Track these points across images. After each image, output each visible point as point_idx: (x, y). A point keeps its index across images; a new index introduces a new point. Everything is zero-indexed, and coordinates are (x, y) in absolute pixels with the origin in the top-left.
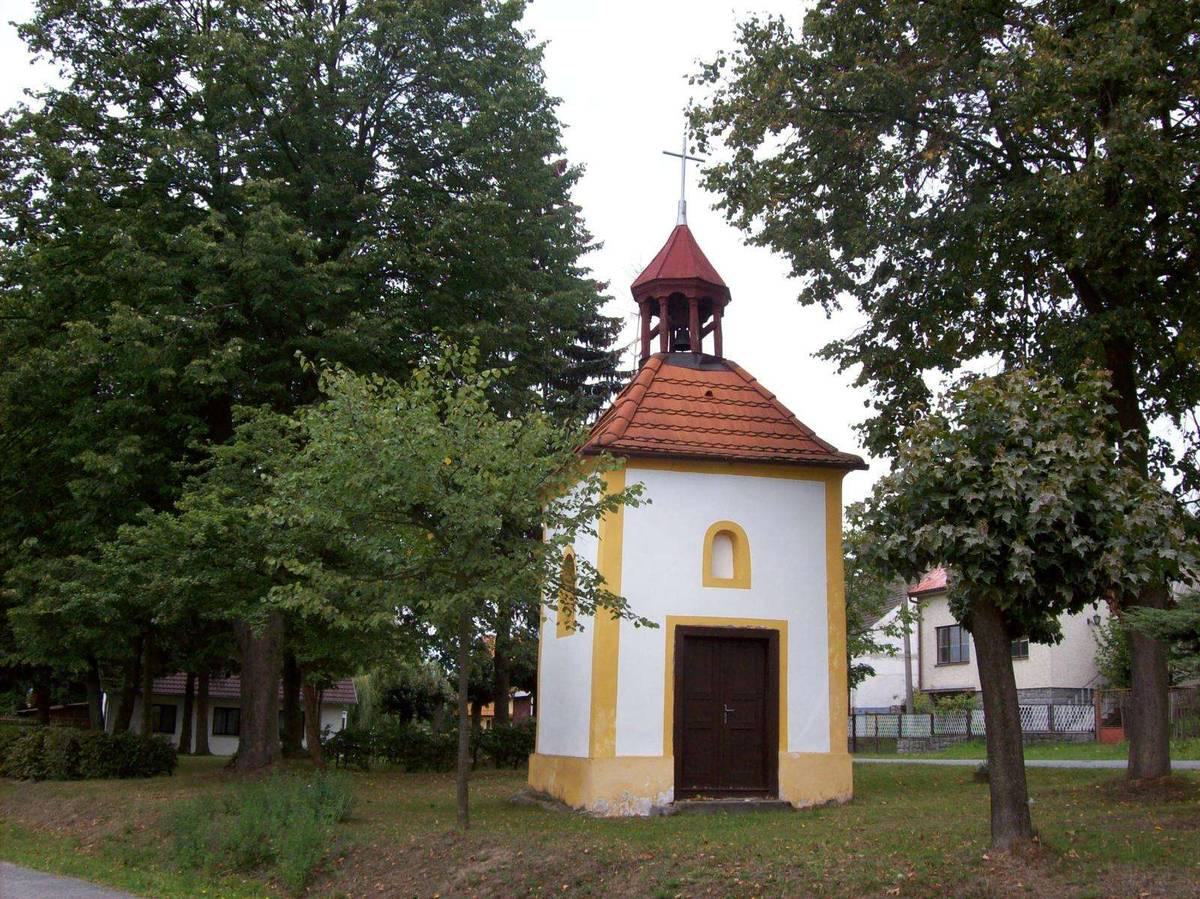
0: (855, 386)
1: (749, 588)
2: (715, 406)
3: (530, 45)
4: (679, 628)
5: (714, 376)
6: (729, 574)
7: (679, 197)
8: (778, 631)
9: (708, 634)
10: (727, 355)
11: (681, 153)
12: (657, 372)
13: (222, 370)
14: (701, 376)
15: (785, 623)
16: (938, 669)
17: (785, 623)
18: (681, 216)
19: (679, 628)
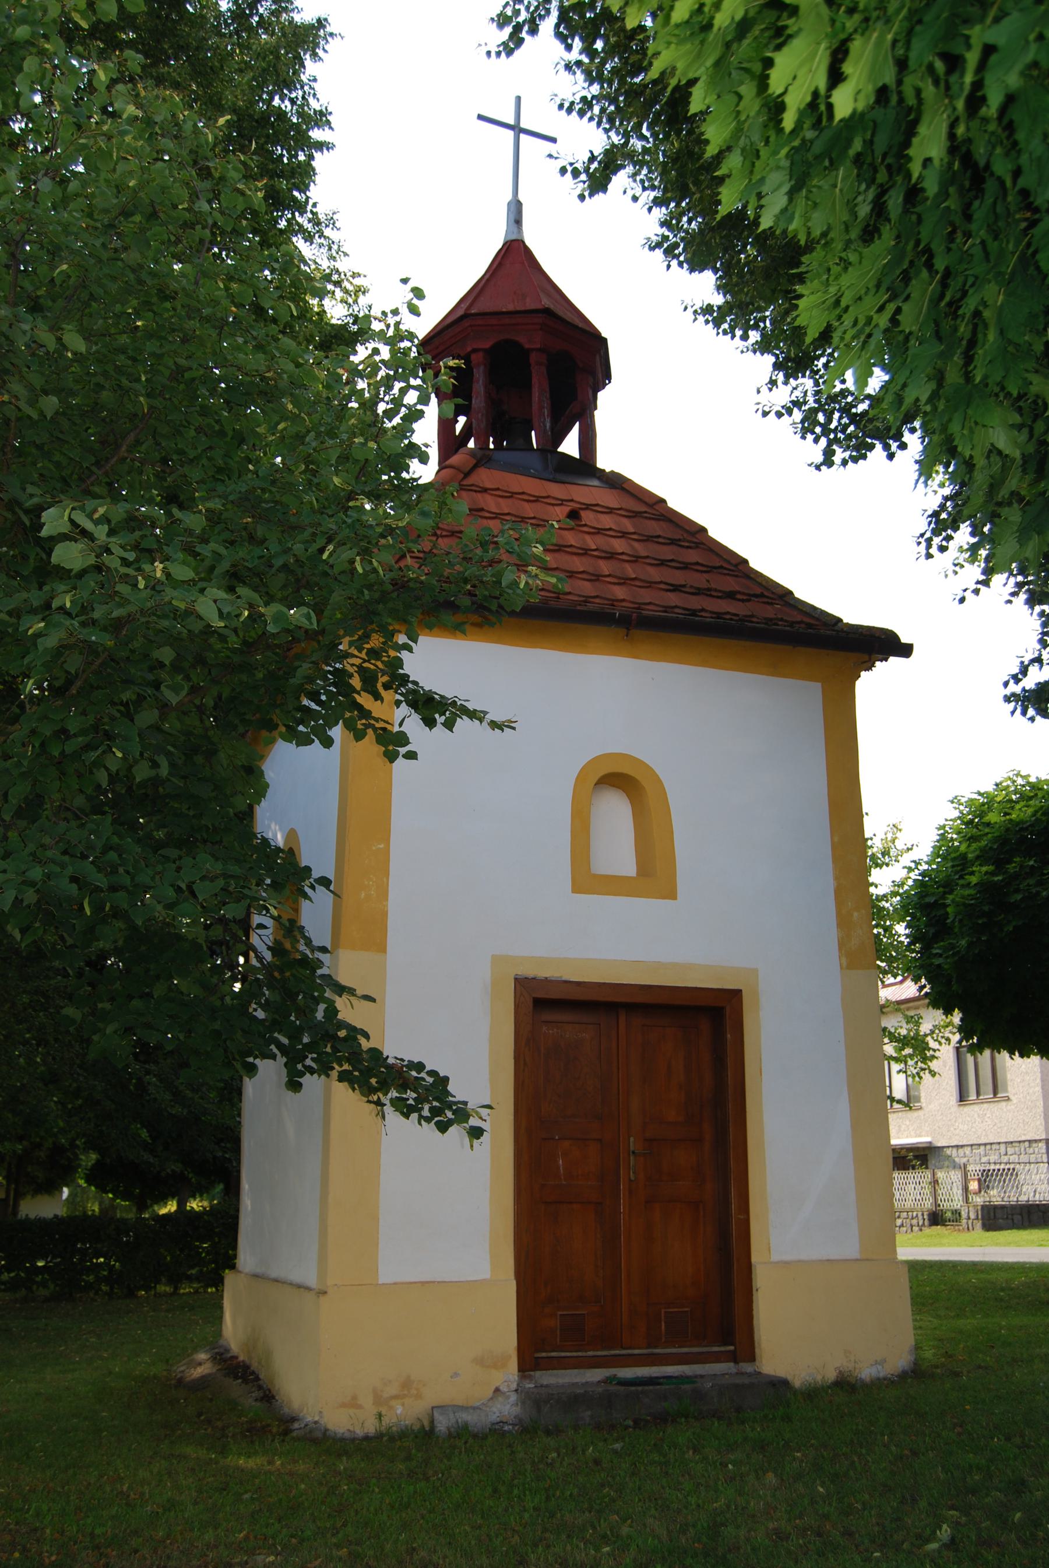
0: (906, 651)
1: (673, 896)
2: (587, 538)
3: (320, 52)
4: (522, 983)
5: (586, 492)
6: (626, 865)
7: (509, 196)
8: (740, 991)
9: (640, 999)
10: (605, 461)
11: (512, 122)
12: (467, 475)
13: (116, 626)
14: (556, 490)
15: (497, 961)
16: (813, 89)
17: (497, 961)
18: (515, 228)
19: (522, 983)
